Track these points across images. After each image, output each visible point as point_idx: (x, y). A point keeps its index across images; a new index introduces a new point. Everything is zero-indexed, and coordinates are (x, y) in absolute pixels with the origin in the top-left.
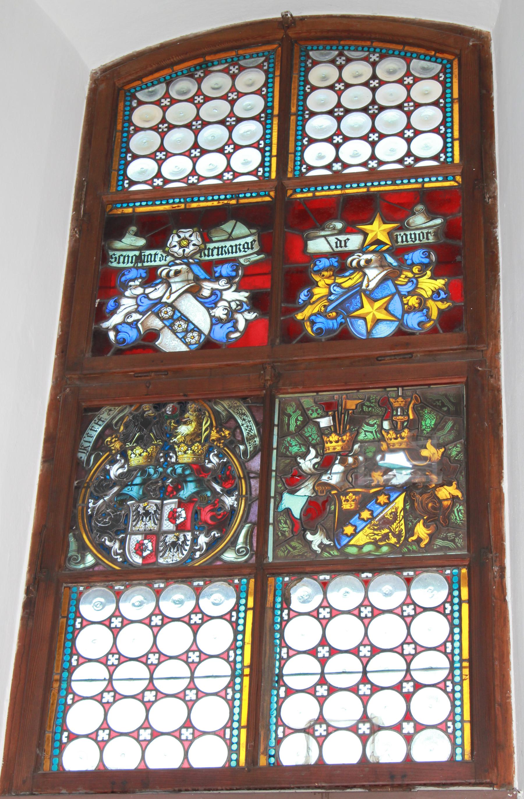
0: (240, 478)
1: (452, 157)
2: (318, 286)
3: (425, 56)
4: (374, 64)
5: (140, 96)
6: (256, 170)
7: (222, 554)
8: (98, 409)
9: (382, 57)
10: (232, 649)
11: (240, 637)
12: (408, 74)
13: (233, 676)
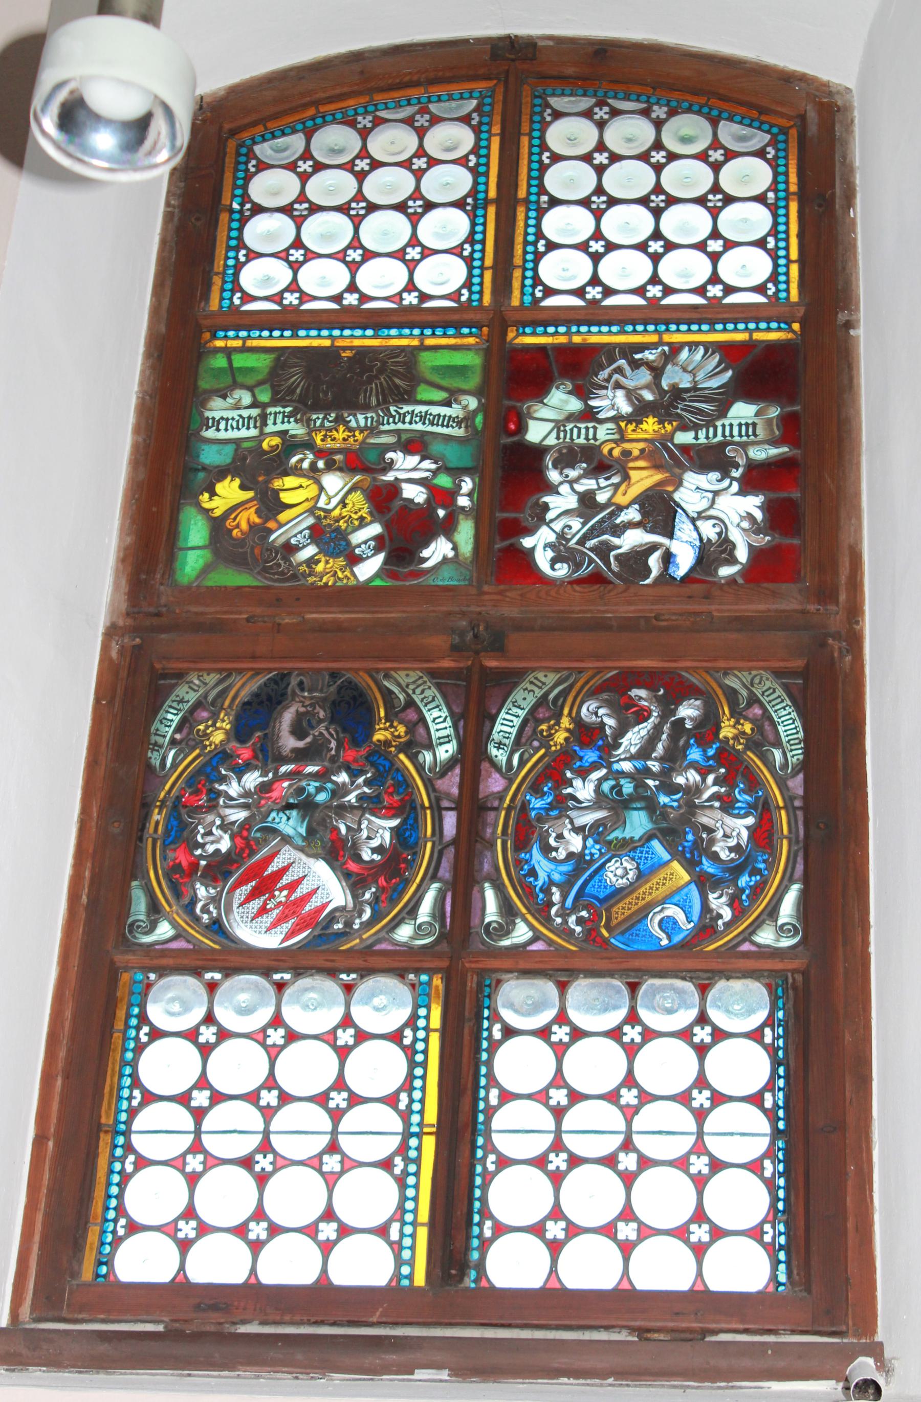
0: (423, 807)
1: (787, 291)
2: (558, 493)
3: (743, 118)
4: (659, 125)
5: (263, 150)
6: (458, 293)
7: (754, 932)
8: (180, 676)
9: (672, 113)
10: (405, 1091)
11: (418, 1072)
12: (716, 144)
13: (407, 1135)
